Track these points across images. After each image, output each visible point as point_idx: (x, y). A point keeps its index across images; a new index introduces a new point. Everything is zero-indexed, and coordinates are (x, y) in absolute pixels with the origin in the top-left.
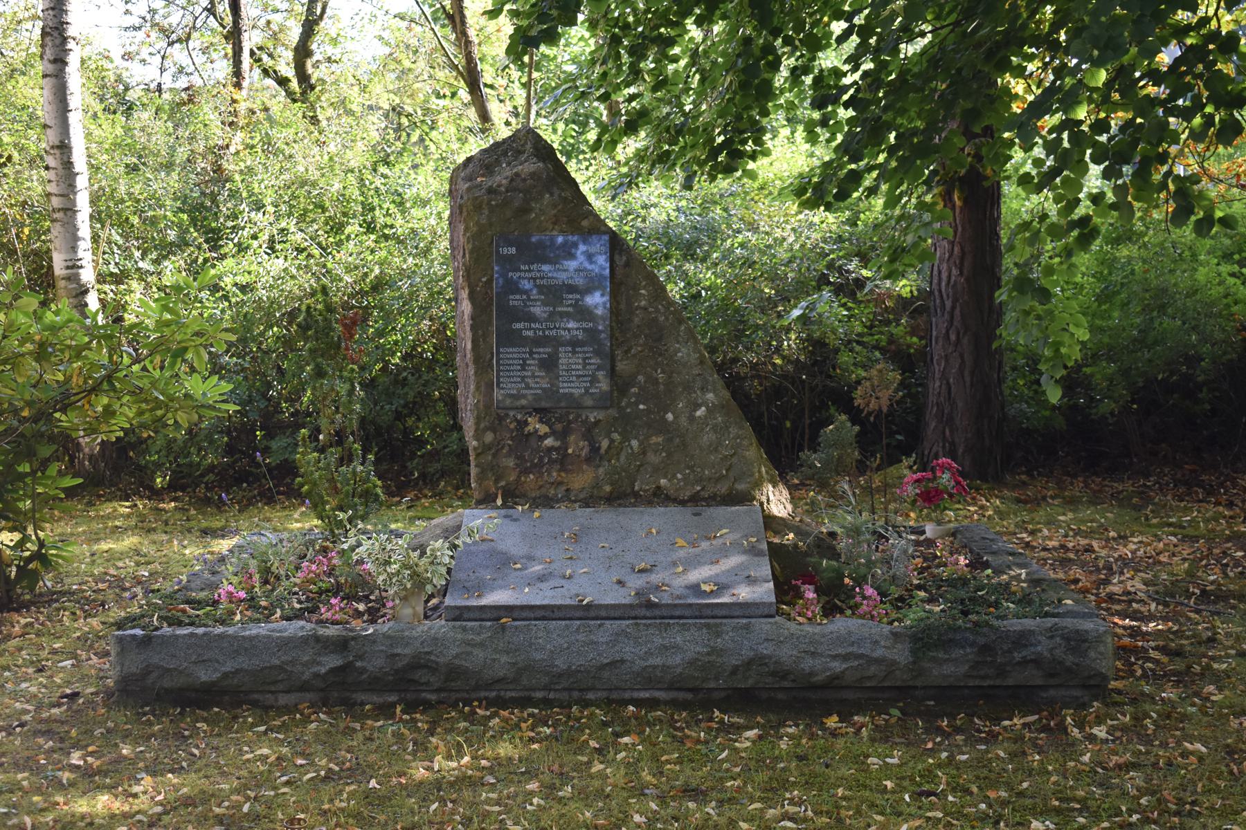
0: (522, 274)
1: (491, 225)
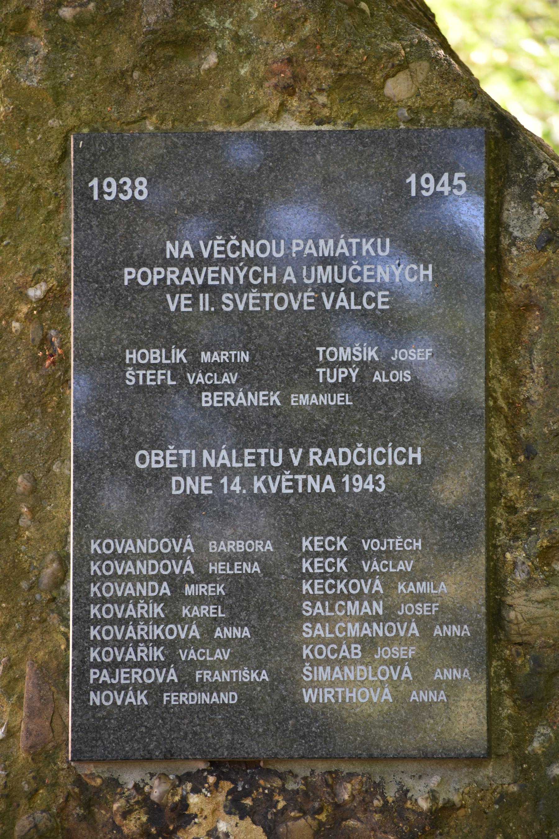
0: (172, 275)
1: (58, 95)
